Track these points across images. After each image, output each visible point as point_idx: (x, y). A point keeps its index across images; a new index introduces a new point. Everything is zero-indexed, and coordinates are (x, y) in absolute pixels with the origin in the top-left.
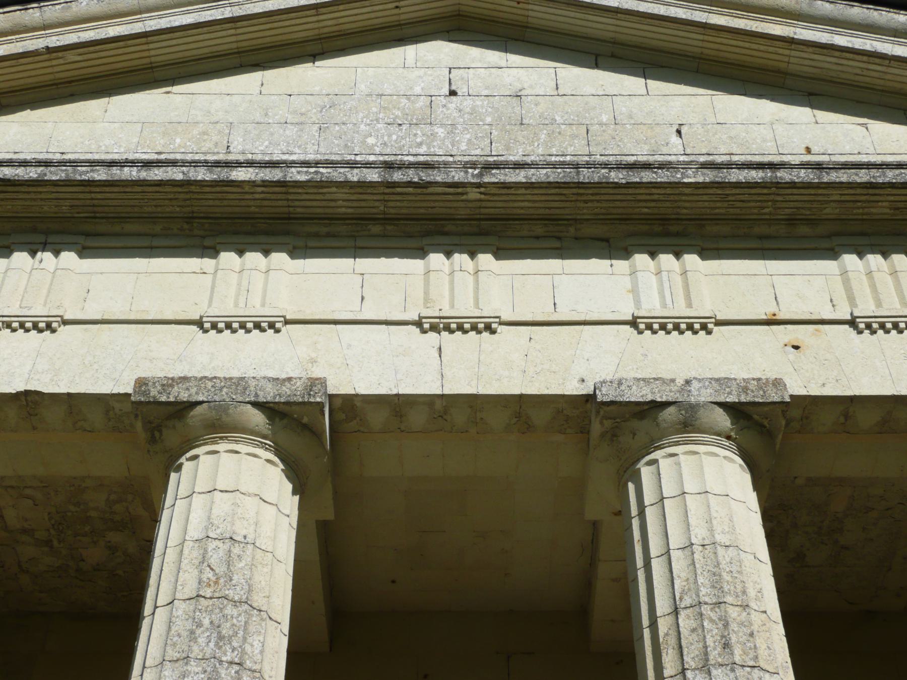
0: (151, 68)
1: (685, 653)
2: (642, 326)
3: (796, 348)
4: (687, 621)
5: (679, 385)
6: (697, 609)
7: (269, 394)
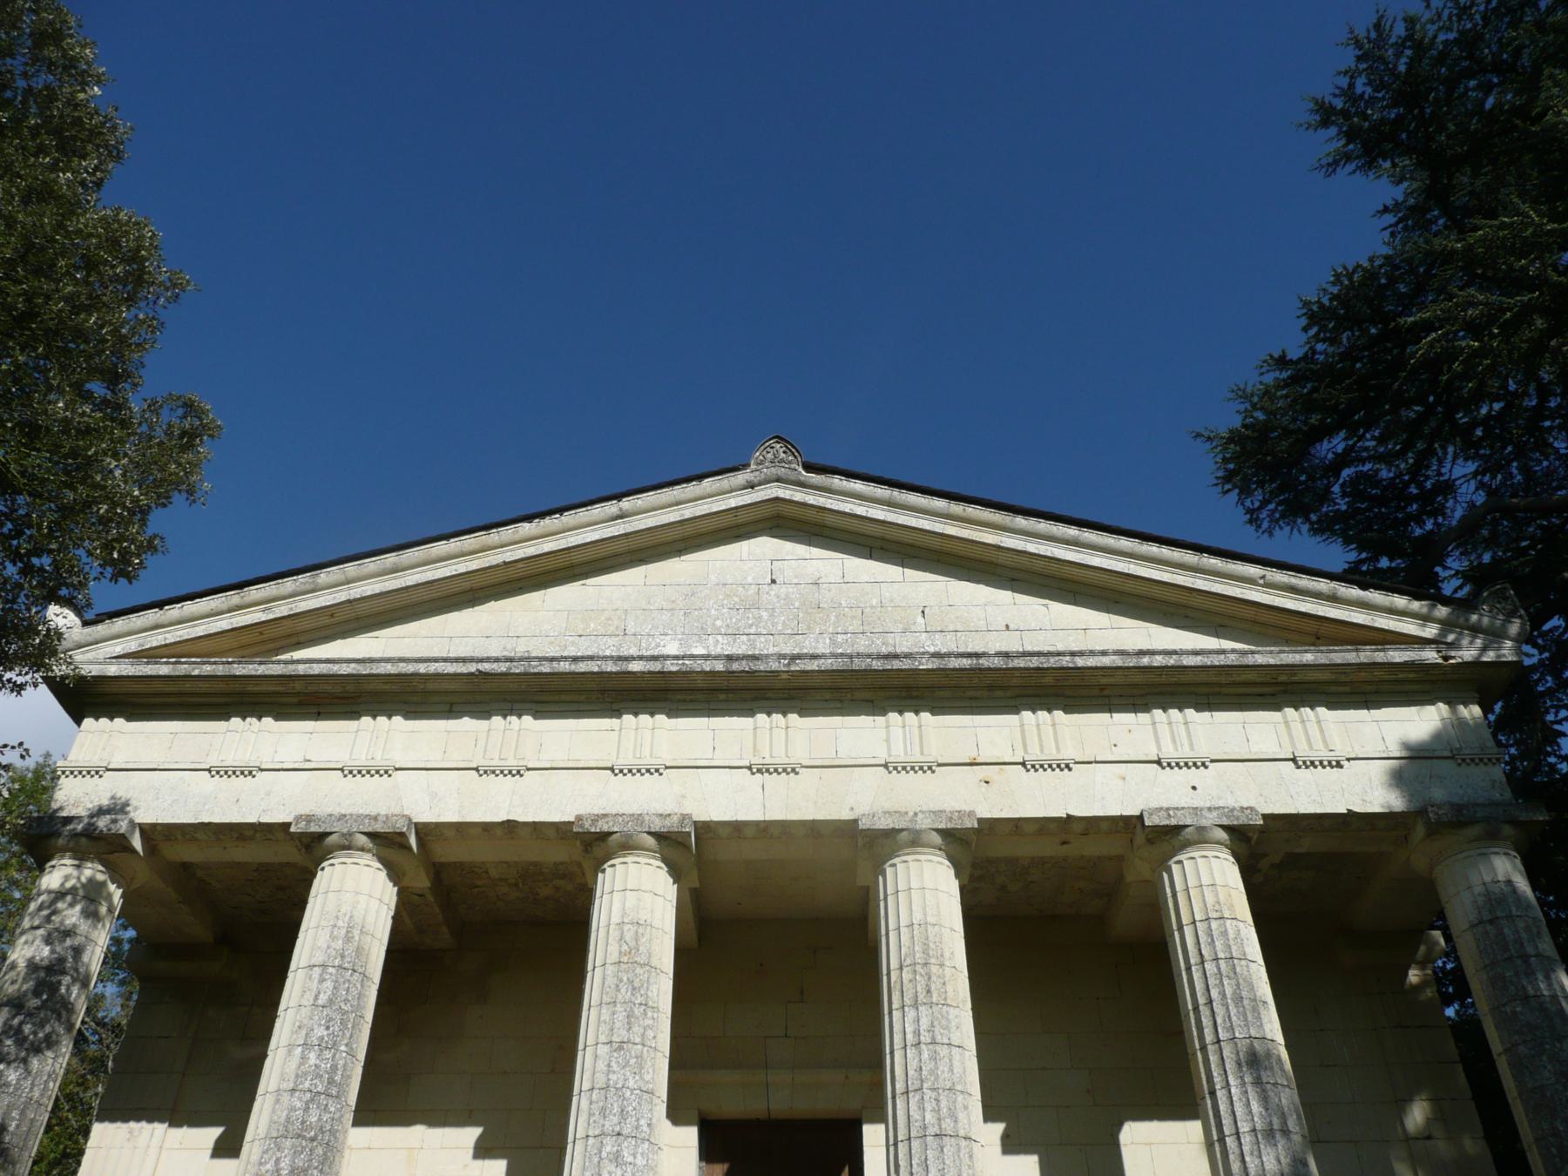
0: (572, 566)
2: (754, 770)
3: (987, 782)
7: (657, 826)
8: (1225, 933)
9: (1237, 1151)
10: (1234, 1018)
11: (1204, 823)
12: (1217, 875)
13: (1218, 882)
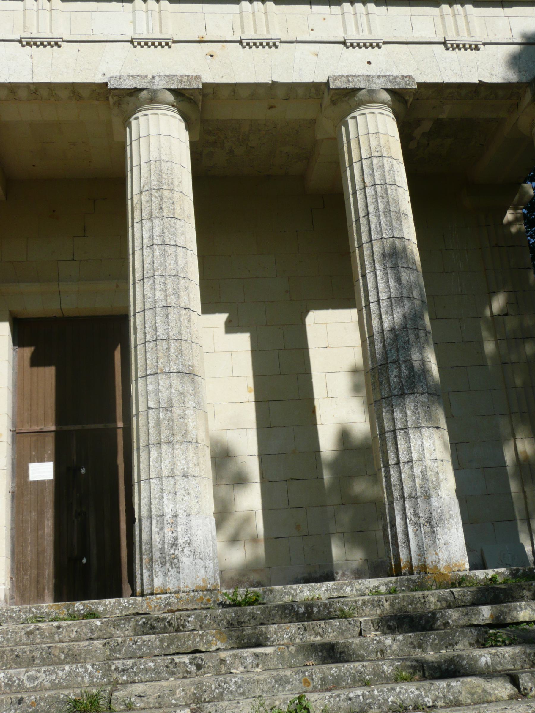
1: (143, 212)
2: (24, 43)
3: (212, 56)
4: (145, 197)
5: (149, 79)
6: (150, 192)
8: (382, 167)
9: (377, 312)
10: (383, 225)
11: (374, 86)
12: (380, 126)
13: (381, 131)
